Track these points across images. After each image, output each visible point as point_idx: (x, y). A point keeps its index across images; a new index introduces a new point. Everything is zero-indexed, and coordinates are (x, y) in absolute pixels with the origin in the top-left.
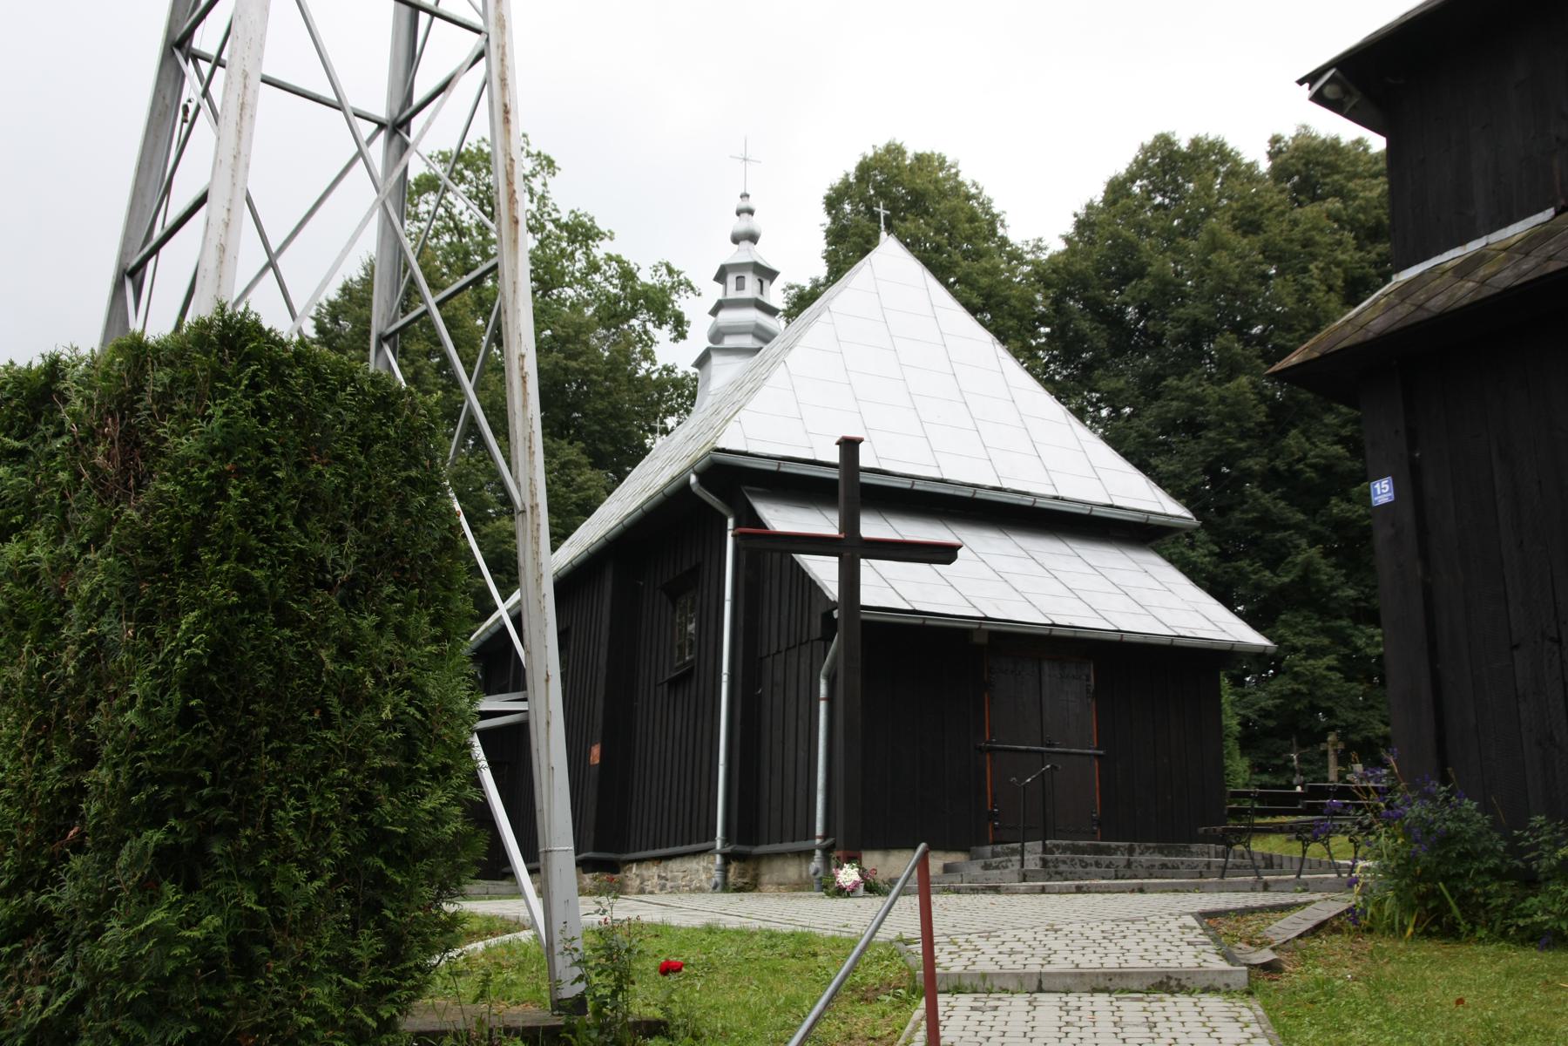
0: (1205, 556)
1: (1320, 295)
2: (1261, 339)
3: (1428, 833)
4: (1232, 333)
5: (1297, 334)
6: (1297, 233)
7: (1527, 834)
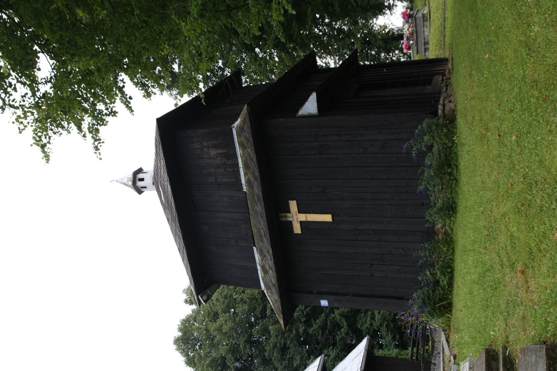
0: (333, 352)
1: (245, 296)
2: (257, 319)
3: (422, 307)
4: (253, 329)
5: (257, 306)
6: (221, 300)
7: (423, 282)
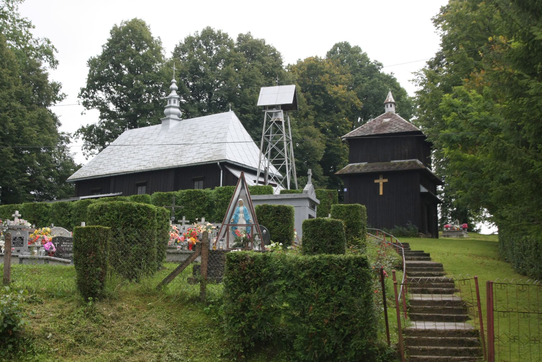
6: (251, 74)
